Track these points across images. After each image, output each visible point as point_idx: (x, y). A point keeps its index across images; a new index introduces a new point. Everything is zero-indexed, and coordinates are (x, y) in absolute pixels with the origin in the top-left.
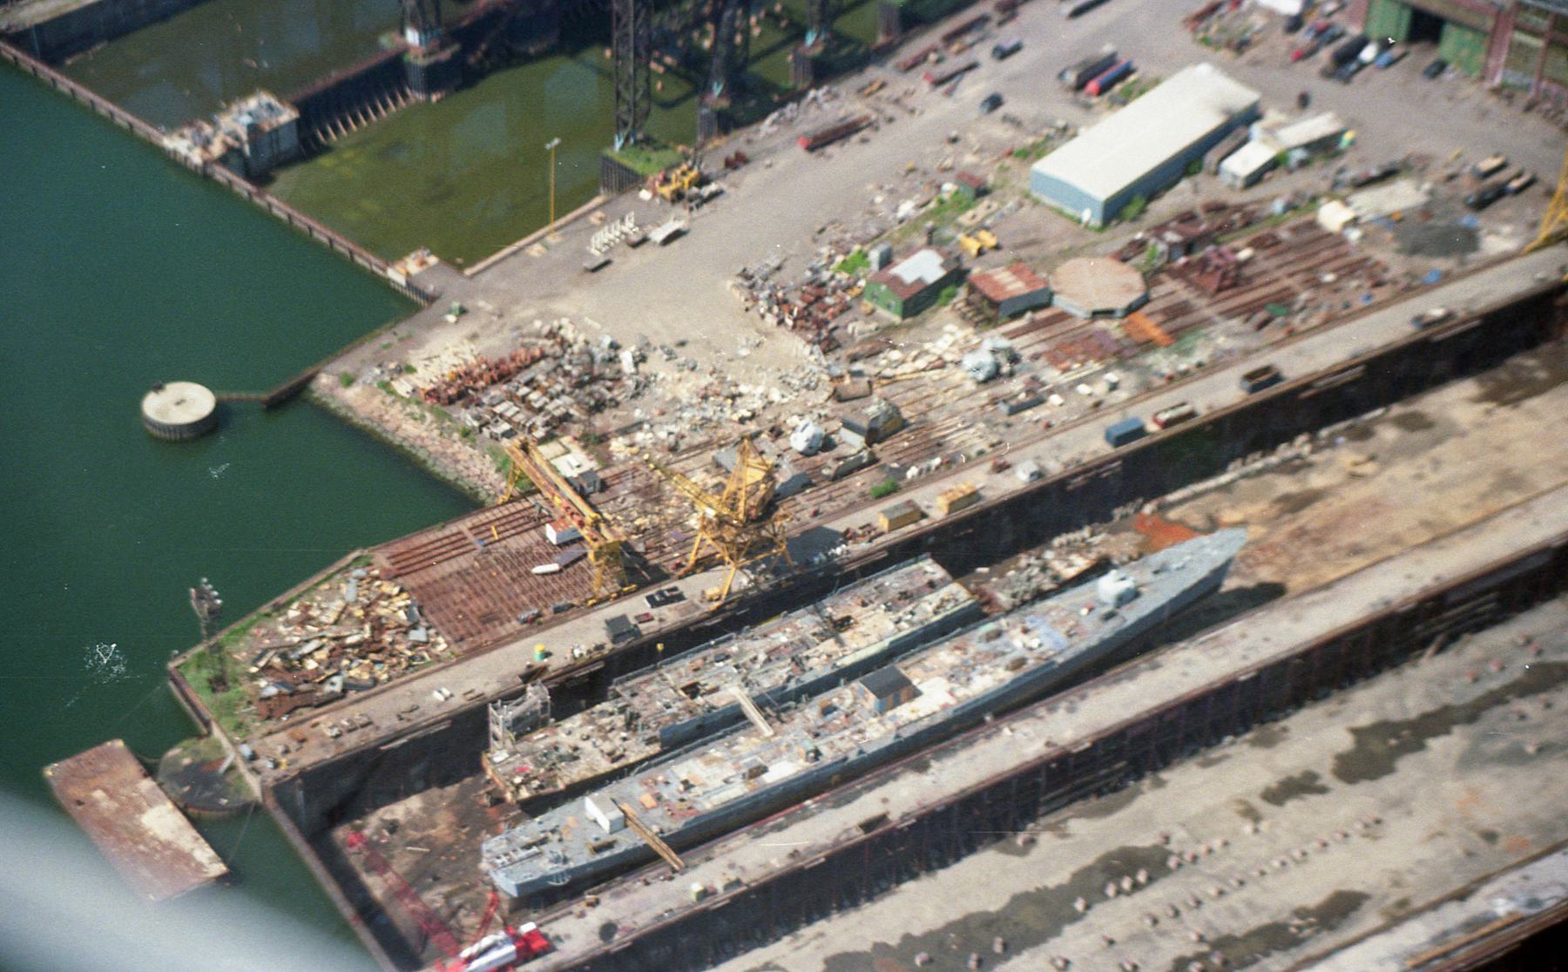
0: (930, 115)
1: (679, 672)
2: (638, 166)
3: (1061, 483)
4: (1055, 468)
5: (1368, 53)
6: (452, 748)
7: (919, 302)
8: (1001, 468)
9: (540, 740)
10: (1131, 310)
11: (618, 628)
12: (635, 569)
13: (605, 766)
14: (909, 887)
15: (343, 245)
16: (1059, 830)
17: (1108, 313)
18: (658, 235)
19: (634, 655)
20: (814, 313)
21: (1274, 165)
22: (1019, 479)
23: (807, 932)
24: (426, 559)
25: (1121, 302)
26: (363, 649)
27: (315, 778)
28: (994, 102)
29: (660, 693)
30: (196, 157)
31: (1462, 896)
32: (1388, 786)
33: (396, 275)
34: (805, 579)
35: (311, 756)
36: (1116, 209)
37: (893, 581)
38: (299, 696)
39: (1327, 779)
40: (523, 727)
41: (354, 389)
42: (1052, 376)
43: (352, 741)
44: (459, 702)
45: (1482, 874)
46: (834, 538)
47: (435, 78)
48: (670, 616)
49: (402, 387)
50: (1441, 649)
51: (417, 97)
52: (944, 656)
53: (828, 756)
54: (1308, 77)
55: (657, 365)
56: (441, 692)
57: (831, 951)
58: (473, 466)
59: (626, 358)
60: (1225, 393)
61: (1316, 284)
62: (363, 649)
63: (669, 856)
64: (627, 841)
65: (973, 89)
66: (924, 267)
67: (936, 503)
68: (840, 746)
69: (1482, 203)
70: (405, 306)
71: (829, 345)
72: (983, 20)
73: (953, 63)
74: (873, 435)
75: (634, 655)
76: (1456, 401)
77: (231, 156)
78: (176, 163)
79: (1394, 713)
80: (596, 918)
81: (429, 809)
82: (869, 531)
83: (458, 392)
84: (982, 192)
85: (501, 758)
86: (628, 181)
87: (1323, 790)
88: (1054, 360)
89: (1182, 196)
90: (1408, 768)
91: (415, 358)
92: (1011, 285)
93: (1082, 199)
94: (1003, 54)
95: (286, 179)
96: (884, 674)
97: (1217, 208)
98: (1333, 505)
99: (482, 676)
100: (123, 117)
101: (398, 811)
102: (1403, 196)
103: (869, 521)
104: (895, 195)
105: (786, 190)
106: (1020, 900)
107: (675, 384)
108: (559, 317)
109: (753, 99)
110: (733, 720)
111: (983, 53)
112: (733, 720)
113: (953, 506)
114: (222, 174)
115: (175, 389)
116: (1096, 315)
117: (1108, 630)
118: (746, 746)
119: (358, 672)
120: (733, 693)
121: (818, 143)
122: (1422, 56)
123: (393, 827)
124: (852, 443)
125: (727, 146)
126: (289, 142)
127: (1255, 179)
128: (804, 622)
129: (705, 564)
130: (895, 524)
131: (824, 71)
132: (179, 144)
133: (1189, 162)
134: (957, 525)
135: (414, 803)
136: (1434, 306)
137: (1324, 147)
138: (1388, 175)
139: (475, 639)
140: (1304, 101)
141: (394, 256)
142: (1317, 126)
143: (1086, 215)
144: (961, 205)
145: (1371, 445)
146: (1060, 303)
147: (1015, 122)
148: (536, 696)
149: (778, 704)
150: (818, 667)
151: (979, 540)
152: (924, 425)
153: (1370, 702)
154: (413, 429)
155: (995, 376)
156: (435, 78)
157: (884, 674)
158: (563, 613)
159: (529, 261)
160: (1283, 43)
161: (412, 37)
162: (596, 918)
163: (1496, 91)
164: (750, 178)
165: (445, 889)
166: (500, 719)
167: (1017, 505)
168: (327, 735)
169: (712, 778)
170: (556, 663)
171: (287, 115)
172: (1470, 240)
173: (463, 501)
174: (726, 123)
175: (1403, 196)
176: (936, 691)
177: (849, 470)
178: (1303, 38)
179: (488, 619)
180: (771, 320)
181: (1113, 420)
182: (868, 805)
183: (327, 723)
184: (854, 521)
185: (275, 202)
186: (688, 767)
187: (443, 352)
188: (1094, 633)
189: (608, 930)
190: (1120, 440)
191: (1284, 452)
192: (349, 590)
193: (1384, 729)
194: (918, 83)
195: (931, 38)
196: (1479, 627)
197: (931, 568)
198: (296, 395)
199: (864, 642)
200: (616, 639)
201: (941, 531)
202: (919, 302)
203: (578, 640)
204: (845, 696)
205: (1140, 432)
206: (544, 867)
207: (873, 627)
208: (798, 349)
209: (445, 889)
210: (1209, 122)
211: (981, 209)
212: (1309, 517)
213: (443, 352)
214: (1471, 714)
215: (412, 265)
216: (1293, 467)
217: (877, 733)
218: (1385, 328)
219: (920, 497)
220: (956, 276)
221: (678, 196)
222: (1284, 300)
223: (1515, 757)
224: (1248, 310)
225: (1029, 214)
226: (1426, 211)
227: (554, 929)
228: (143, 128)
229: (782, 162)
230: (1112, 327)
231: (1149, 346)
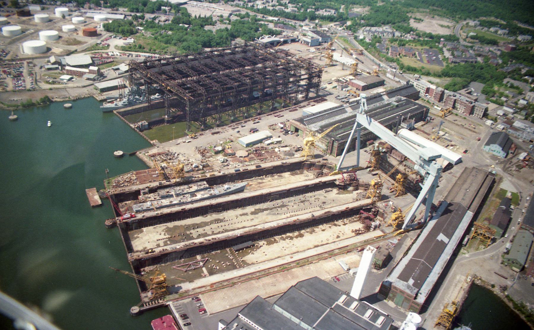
1: (167, 190)
2: (188, 133)
3: (227, 175)
4: (226, 173)
5: (289, 132)
6: (134, 196)
7: (217, 153)
8: (220, 172)
9: (146, 195)
10: (245, 157)
11: (160, 184)
12: (166, 178)
13: (153, 199)
14: (188, 219)
15: (147, 138)
16: (211, 215)
17: (242, 157)
18: (187, 141)
19: (162, 187)
20: (203, 153)
21: (272, 143)
22: (221, 174)
23: (173, 222)
24: (141, 173)
25: (243, 156)
27: (117, 195)
28: (239, 132)
29: (163, 192)
31: (255, 226)
32: (257, 216)
33: (152, 142)
34: (188, 182)
35: (116, 193)
36: (248, 145)
37: (199, 183)
38: (118, 185)
39: (249, 214)
40: (145, 193)
41: (142, 155)
42: (231, 163)
43: (122, 191)
44: (137, 189)
46: (193, 177)
47: (168, 122)
48: (168, 183)
49: (146, 154)
50: (271, 201)
51: (166, 124)
52: (202, 192)
53: (182, 201)
54: (281, 134)
55: (180, 156)
56: (135, 188)
58: (151, 164)
59: (176, 154)
60: (253, 168)
61: (271, 157)
63: (155, 210)
64: (151, 207)
65: (237, 130)
66: (220, 148)
67: (208, 175)
68: (184, 200)
69: (296, 151)
70: (152, 146)
71: (203, 156)
73: (236, 127)
74: (204, 166)
75: (162, 187)
76: (287, 175)
77: (138, 127)
78: (131, 127)
79: (261, 208)
80: (143, 215)
82: (198, 177)
83: (154, 156)
84: (232, 141)
85: (141, 197)
86: (187, 135)
88: (232, 161)
89: (259, 145)
90: (260, 214)
91: (150, 152)
92: (230, 151)
93: (244, 143)
94: (242, 127)
95: (145, 132)
96: (193, 194)
97: (263, 147)
98: (265, 184)
99: (141, 187)
100: (127, 122)
101: (127, 202)
102: (287, 149)
103: (198, 175)
104: (221, 140)
105: (207, 139)
106: (202, 222)
107: (181, 158)
109: (207, 127)
110: (172, 196)
111: (240, 126)
112: (172, 196)
113: (210, 175)
114: (136, 129)
115: (119, 151)
116: (240, 157)
117: (225, 192)
118: (171, 199)
119: (126, 184)
120: (173, 193)
121: (213, 134)
122: (296, 134)
123: (126, 204)
124: (201, 167)
125: (201, 133)
126: (147, 127)
127: (269, 144)
128: (186, 186)
129: (174, 178)
130: (202, 176)
131: (218, 126)
132: (132, 125)
133: (261, 141)
134: (211, 178)
135: (130, 202)
136: (284, 161)
137: (279, 142)
138: (286, 146)
139: (141, 183)
140: (279, 137)
141: (152, 140)
142: (279, 139)
144: (229, 142)
145: (273, 178)
146: (236, 155)
148: (147, 190)
149: (178, 195)
150: (185, 192)
151: (213, 181)
152: (212, 166)
153: (258, 206)
154: (146, 159)
155: (224, 162)
156: (168, 122)
157: (193, 194)
158: (154, 181)
160: (280, 130)
161: (166, 116)
162: (143, 215)
164: (202, 136)
166: (142, 192)
167: (220, 177)
168: (119, 190)
169: (166, 202)
170: (151, 187)
171: (147, 123)
172: (293, 155)
173: (148, 167)
174: (203, 130)
175: (287, 149)
176: (199, 196)
177: (200, 170)
178: (282, 130)
179: (145, 181)
181: (237, 169)
182: (183, 207)
183: (120, 189)
184: (197, 176)
186: (163, 201)
187: (154, 151)
188: (223, 192)
189: (143, 216)
190: (236, 171)
191: (261, 177)
192: (129, 175)
193: (260, 209)
194: (230, 129)
195: (234, 124)
196: (277, 199)
197: (205, 183)
198: (134, 154)
199: (192, 190)
200: (160, 184)
201: (208, 178)
202: (217, 153)
203: (155, 184)
204: (187, 195)
205: (239, 170)
206: (140, 209)
207: (194, 188)
208: (199, 156)
210: (265, 137)
211: (231, 143)
212: (261, 185)
213: (154, 151)
214: (271, 209)
215: (154, 141)
216: (261, 179)
217: (189, 200)
218: (278, 163)
219: (206, 174)
220: (223, 150)
221: (192, 138)
222: (266, 158)
223: (273, 214)
224: (260, 159)
225: (237, 145)
226: (289, 151)
227: (137, 215)
229: (208, 135)
230: (242, 159)
231: (246, 161)
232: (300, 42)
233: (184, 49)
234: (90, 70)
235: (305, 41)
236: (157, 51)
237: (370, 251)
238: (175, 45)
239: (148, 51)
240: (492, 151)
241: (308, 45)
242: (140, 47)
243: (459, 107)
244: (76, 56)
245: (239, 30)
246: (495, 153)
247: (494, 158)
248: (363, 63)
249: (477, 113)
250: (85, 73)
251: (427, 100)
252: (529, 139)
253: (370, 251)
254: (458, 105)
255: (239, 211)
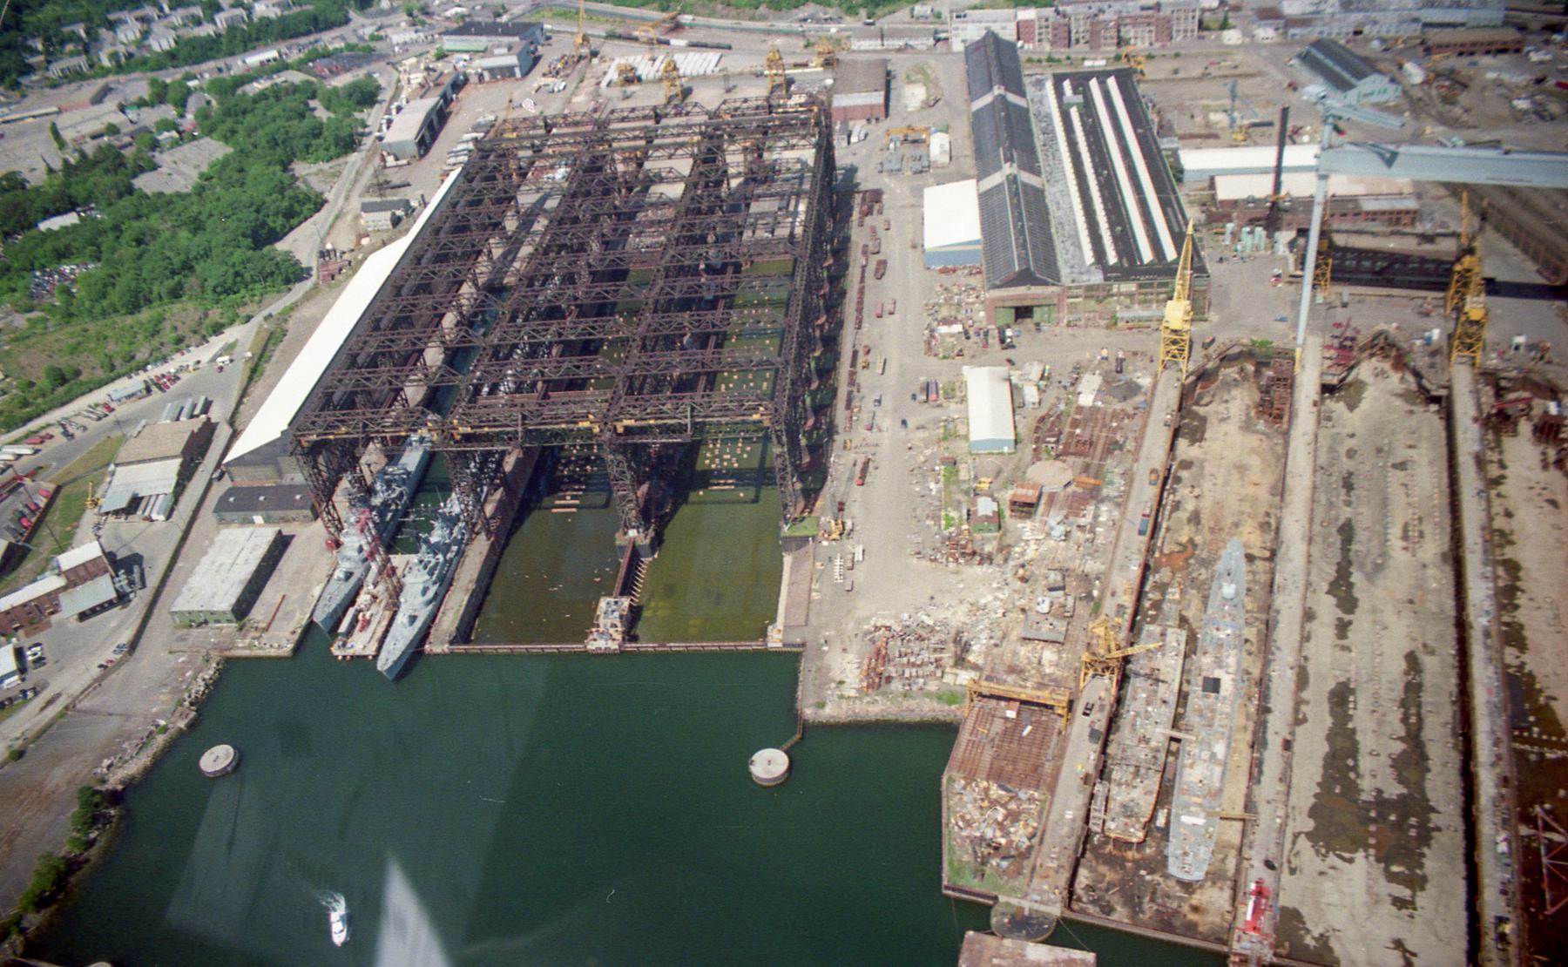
0: (886, 441)
26: (1403, 818)
30: (614, 646)
45: (139, 650)
57: (1306, 810)
62: (1403, 818)
72: (850, 393)
81: (1092, 870)
87: (1350, 623)
108: (868, 618)
122: (1029, 323)
143: (1006, 450)
147: (921, 427)
156: (657, 542)
159: (820, 602)
163: (1068, 325)
165: (1147, 899)
180: (952, 566)
185: (646, 645)
209: (1147, 899)
228: (578, 647)
232: (474, 79)
233: (227, 292)
234: (67, 574)
235: (491, 70)
236: (141, 355)
237: (1250, 577)
238: (176, 294)
239: (100, 373)
240: (1366, 95)
241: (512, 74)
242: (61, 378)
243: (1131, 34)
244: (203, 530)
245: (280, 137)
246: (1375, 99)
247: (1382, 107)
248: (730, 48)
249: (1182, 27)
250: (52, 597)
251: (1044, 57)
252: (1351, 30)
253: (1250, 577)
254: (1129, 32)
255: (1453, 661)
